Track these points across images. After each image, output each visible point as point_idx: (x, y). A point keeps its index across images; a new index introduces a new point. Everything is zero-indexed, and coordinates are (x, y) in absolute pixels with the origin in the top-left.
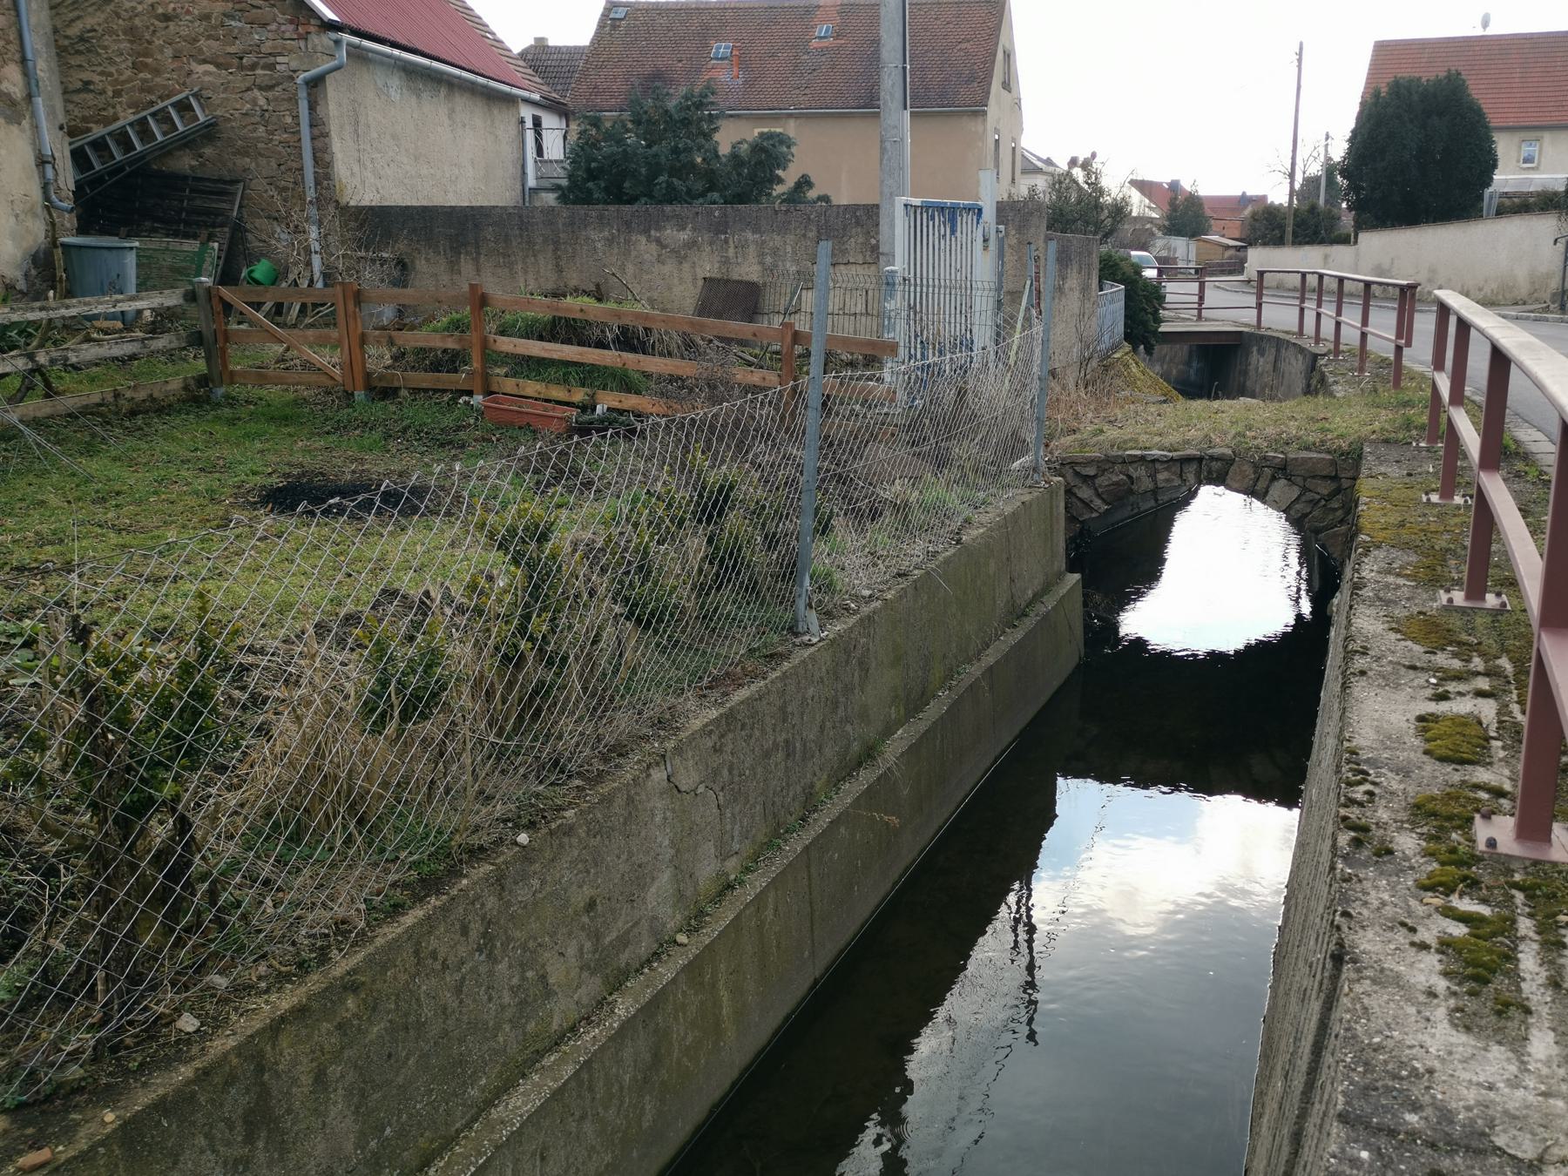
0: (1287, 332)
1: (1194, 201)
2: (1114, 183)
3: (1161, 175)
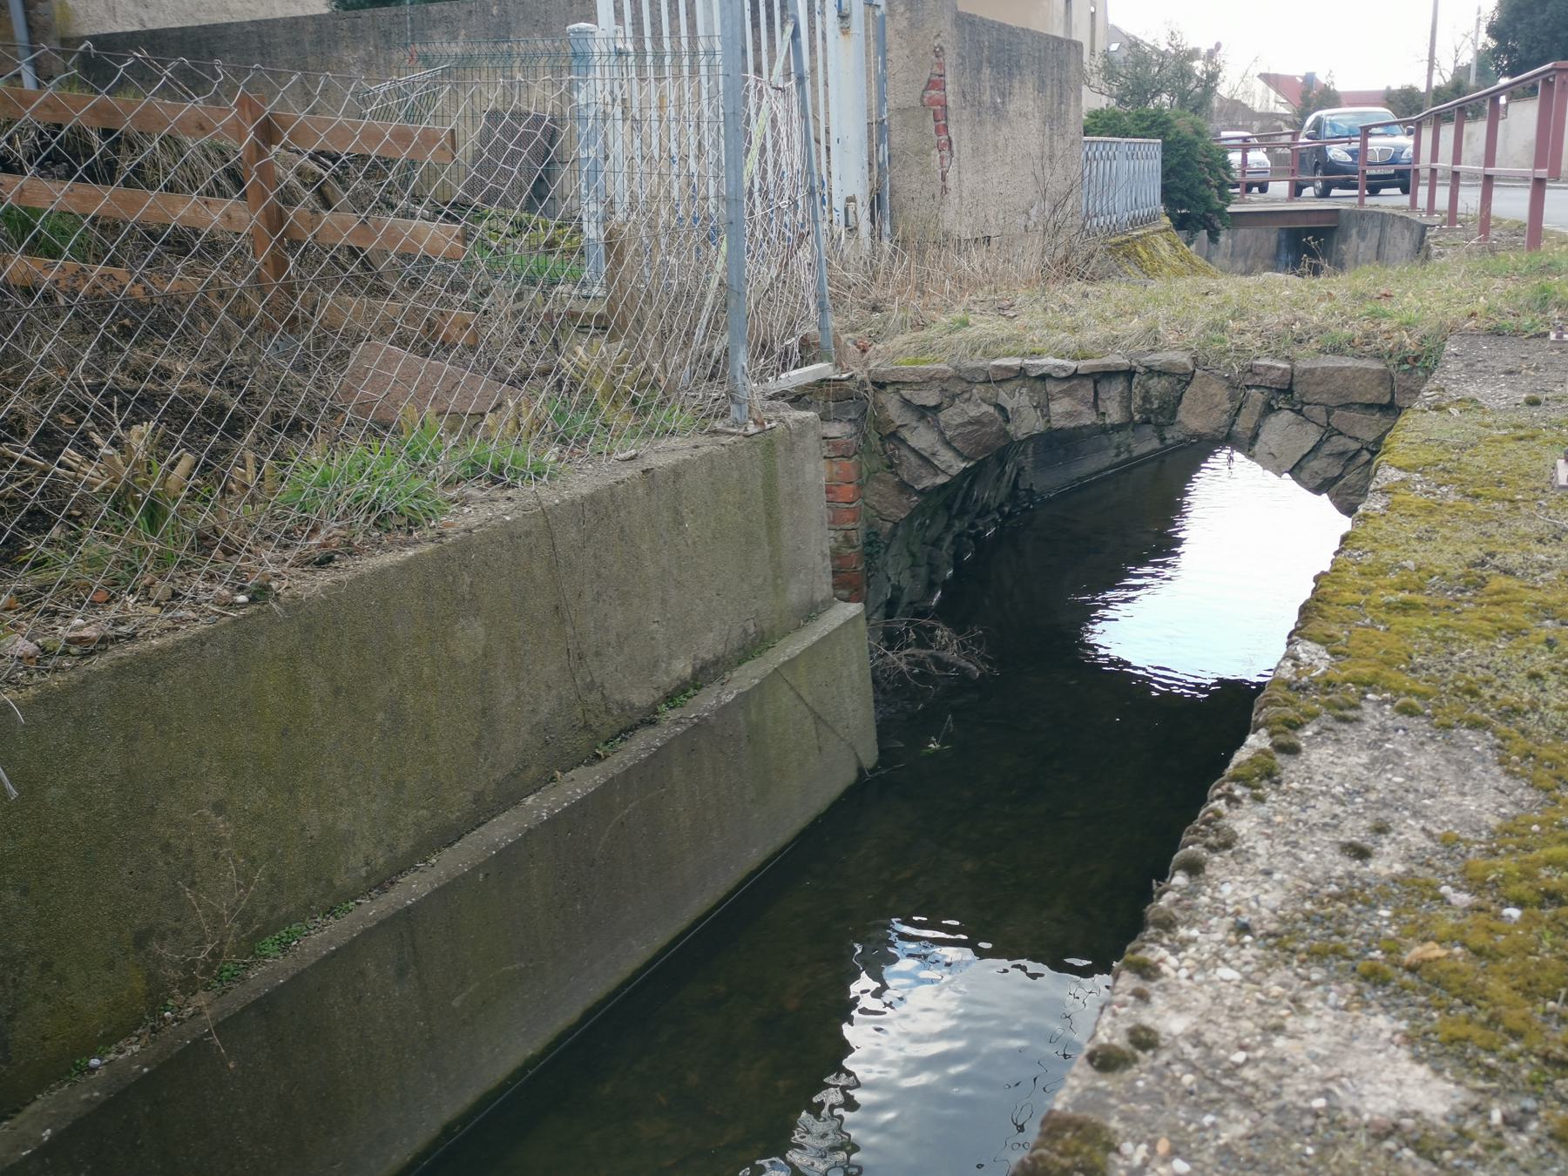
2: (1240, 82)
3: (1294, 67)
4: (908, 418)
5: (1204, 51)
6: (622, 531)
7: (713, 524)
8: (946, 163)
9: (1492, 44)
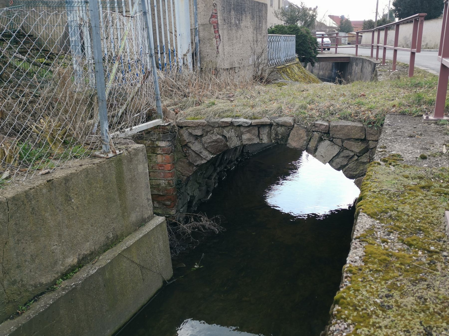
0: (367, 57)
1: (348, 21)
2: (323, 17)
3: (338, 14)
4: (192, 139)
5: (313, 9)
6: (33, 209)
7: (88, 197)
8: (218, 43)
9: (394, 8)
